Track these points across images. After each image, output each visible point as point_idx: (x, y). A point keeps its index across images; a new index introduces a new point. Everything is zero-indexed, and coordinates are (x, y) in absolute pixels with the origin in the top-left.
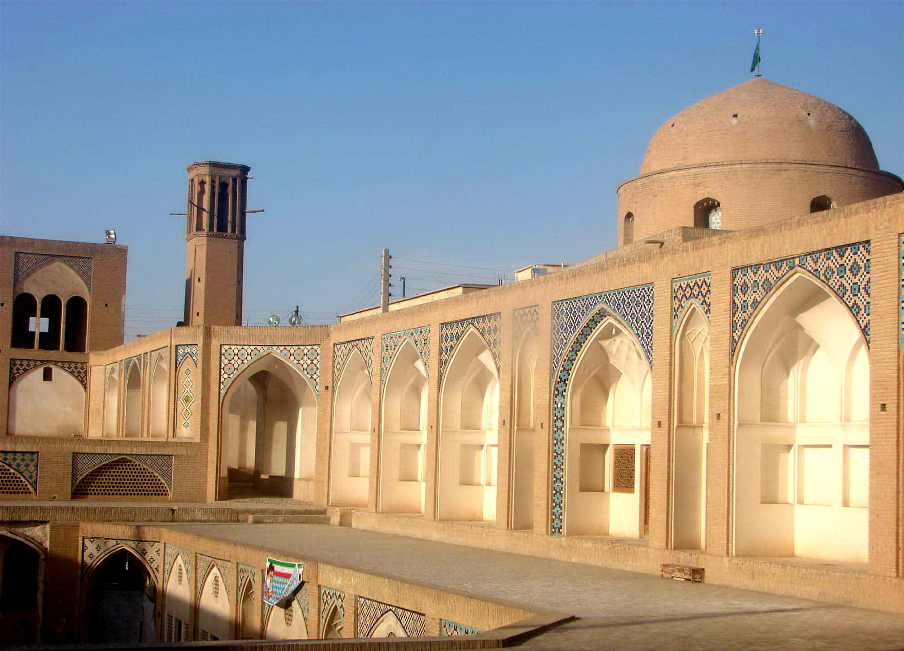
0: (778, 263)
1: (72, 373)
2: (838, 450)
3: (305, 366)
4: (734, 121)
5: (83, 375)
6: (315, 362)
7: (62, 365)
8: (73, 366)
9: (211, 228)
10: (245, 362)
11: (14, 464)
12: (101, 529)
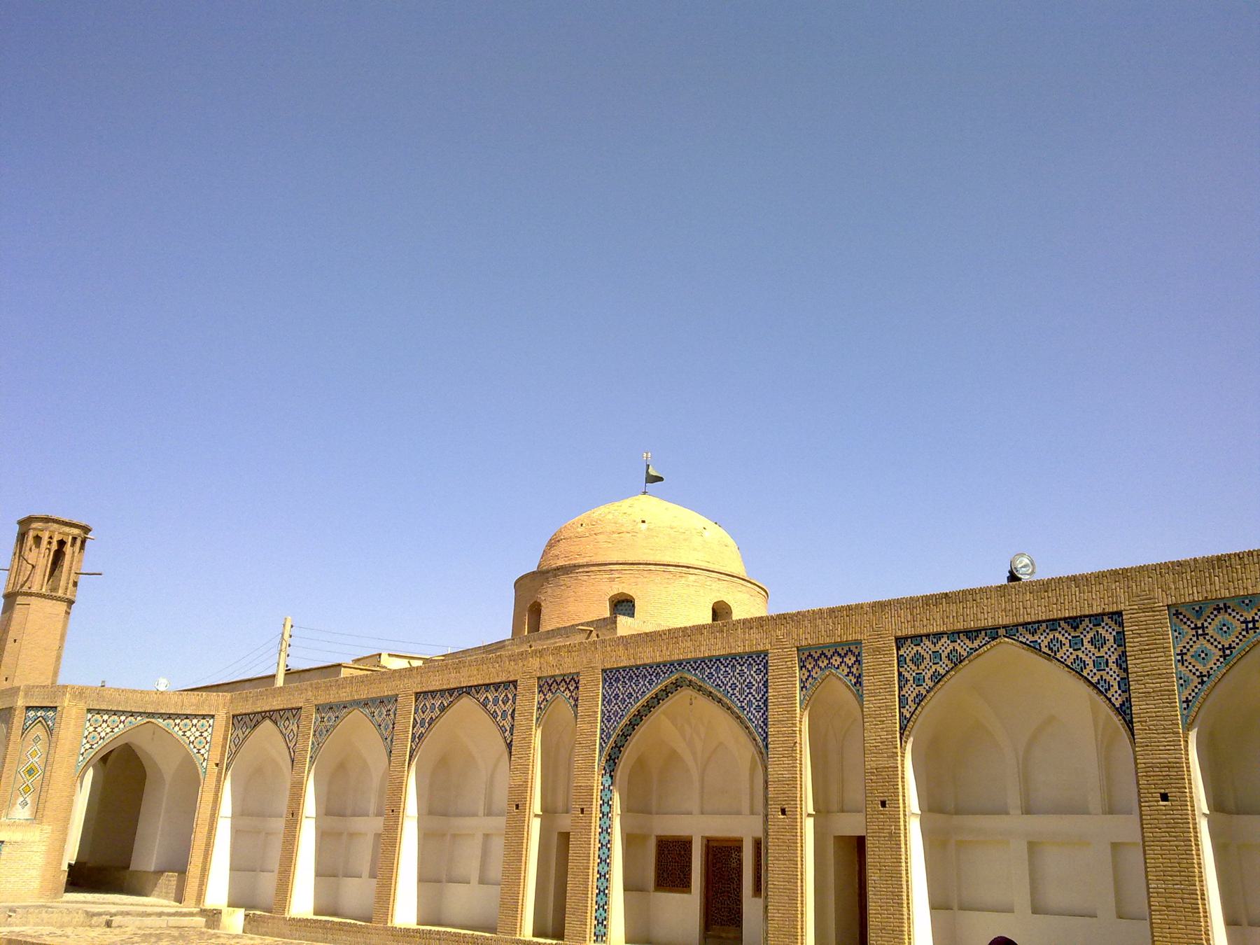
0: (971, 634)
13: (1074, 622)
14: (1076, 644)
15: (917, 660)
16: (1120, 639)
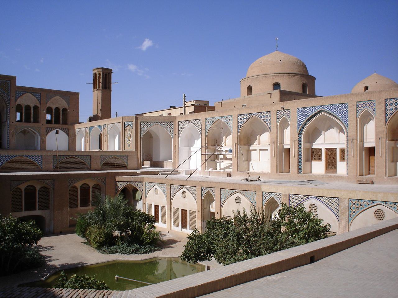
1: (64, 131)
2: (258, 150)
3: (168, 128)
4: (279, 60)
5: (67, 132)
6: (171, 127)
7: (61, 129)
8: (65, 129)
9: (103, 88)
10: (149, 127)
11: (84, 159)
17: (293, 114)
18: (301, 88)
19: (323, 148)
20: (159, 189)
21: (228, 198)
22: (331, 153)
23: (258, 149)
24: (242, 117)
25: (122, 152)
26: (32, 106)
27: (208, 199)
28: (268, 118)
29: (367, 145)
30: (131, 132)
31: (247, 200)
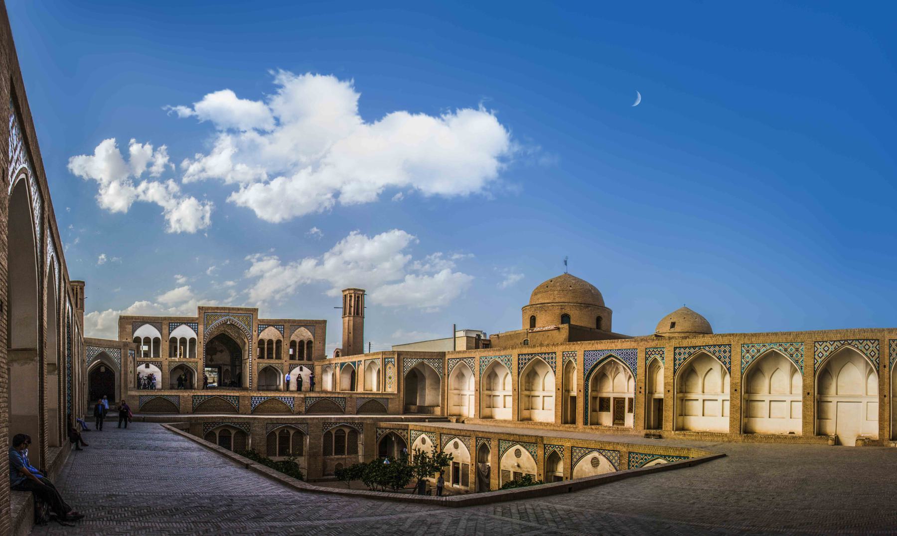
7: (306, 365)
12: (383, 424)
13: (720, 346)
14: (719, 351)
15: (680, 354)
16: (730, 352)
17: (580, 357)
18: (595, 321)
19: (612, 396)
20: (428, 440)
21: (506, 450)
22: (619, 402)
23: (701, 397)
24: (524, 357)
25: (382, 394)
26: (274, 340)
27: (483, 451)
28: (727, 354)
29: (657, 396)
30: (392, 372)
31: (527, 453)
